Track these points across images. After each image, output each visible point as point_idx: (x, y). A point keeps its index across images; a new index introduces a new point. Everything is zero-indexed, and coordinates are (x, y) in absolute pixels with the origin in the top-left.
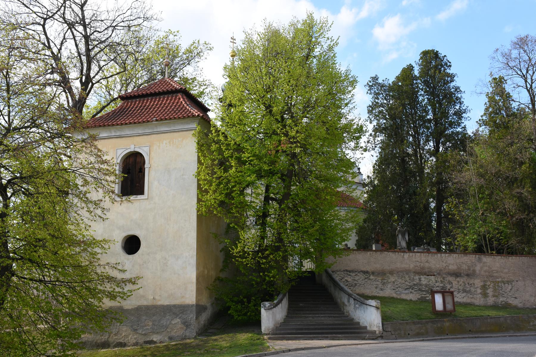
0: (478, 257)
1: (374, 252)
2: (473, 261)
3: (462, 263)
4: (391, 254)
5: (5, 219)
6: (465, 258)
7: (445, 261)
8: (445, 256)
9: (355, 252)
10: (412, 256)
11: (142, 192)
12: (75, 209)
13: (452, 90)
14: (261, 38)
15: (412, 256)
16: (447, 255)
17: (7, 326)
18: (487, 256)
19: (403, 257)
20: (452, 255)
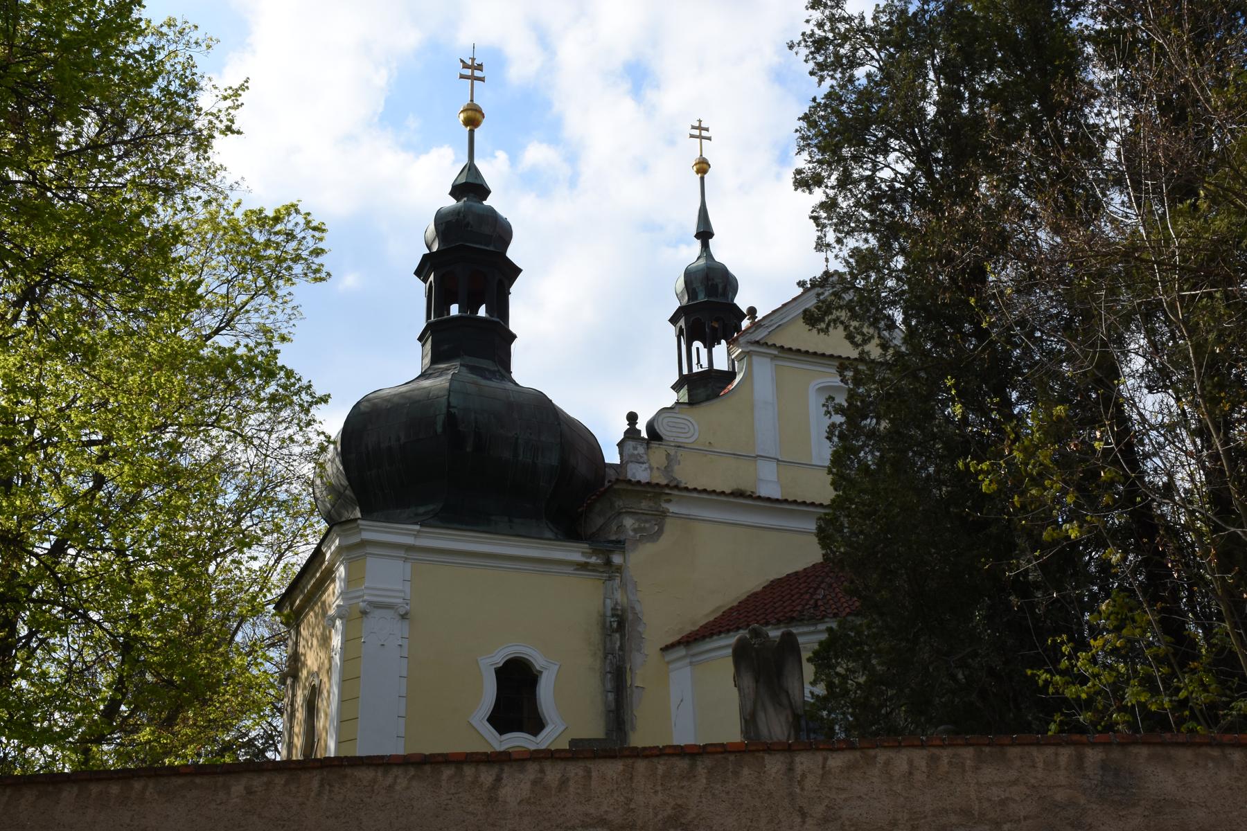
0: (1104, 766)
1: (280, 780)
2: (1060, 796)
3: (966, 812)
4: (402, 783)
5: (617, 559)
6: (989, 773)
7: (819, 810)
8: (825, 773)
9: (138, 785)
10: (564, 782)
11: (519, 271)
12: (202, 681)
13: (874, 350)
14: (265, 343)
15: (564, 782)
16: (836, 761)
17: (971, 221)
18: (1186, 754)
19: (492, 797)
20: (882, 756)
